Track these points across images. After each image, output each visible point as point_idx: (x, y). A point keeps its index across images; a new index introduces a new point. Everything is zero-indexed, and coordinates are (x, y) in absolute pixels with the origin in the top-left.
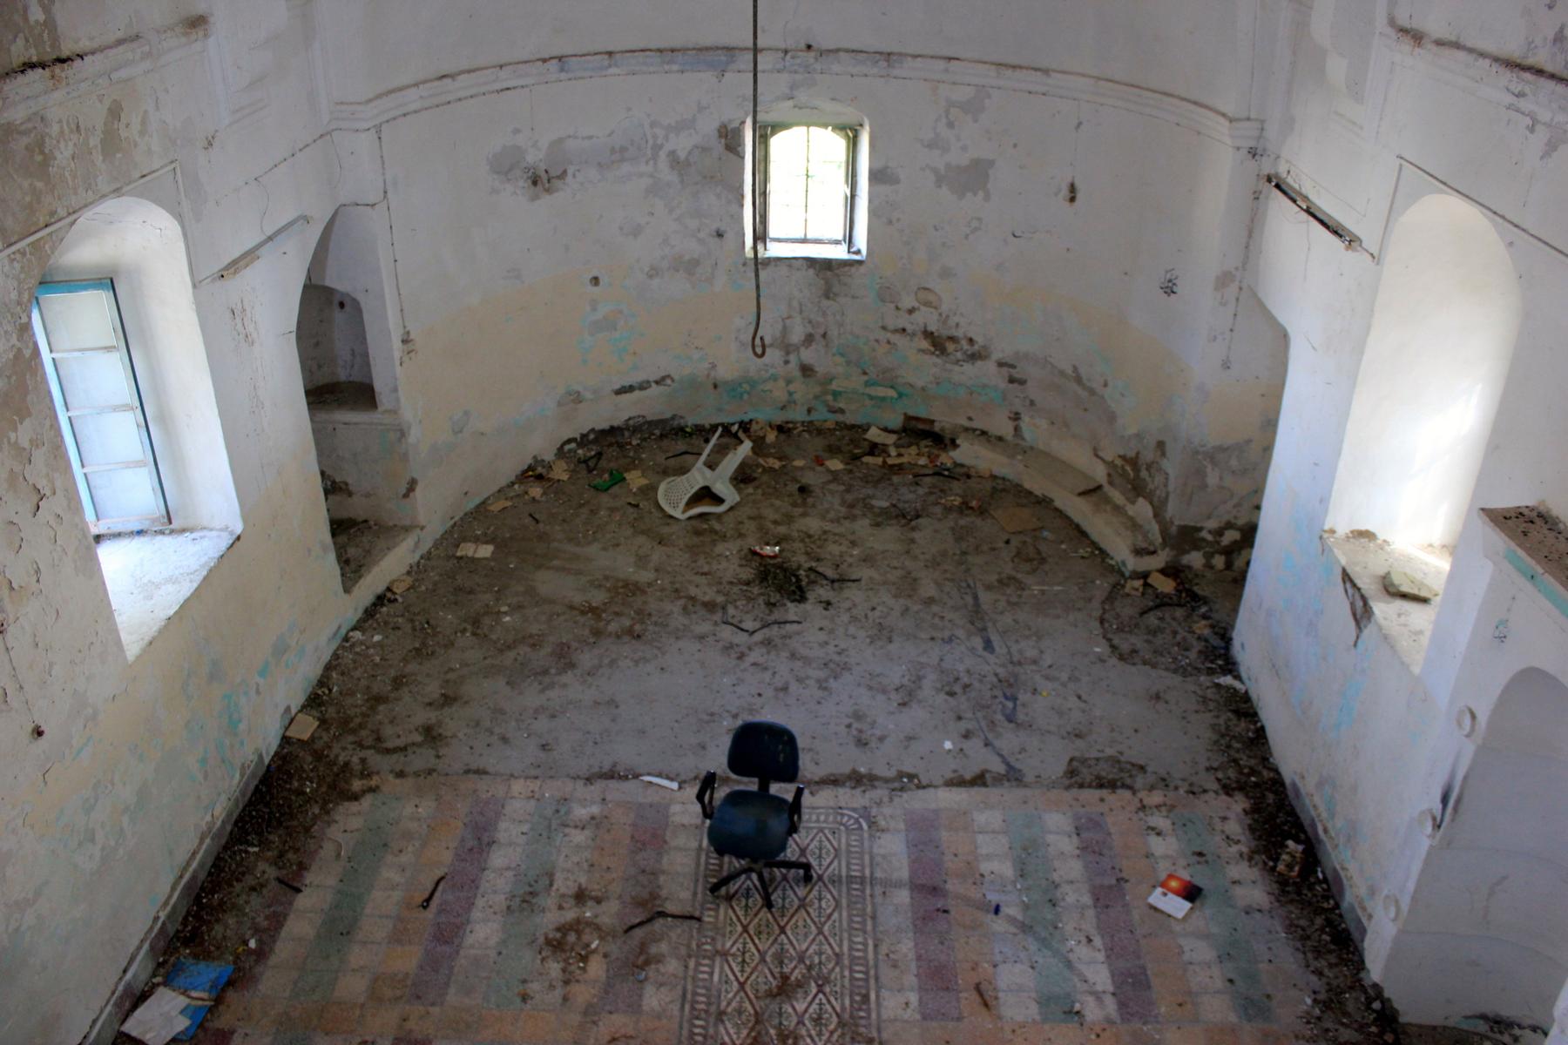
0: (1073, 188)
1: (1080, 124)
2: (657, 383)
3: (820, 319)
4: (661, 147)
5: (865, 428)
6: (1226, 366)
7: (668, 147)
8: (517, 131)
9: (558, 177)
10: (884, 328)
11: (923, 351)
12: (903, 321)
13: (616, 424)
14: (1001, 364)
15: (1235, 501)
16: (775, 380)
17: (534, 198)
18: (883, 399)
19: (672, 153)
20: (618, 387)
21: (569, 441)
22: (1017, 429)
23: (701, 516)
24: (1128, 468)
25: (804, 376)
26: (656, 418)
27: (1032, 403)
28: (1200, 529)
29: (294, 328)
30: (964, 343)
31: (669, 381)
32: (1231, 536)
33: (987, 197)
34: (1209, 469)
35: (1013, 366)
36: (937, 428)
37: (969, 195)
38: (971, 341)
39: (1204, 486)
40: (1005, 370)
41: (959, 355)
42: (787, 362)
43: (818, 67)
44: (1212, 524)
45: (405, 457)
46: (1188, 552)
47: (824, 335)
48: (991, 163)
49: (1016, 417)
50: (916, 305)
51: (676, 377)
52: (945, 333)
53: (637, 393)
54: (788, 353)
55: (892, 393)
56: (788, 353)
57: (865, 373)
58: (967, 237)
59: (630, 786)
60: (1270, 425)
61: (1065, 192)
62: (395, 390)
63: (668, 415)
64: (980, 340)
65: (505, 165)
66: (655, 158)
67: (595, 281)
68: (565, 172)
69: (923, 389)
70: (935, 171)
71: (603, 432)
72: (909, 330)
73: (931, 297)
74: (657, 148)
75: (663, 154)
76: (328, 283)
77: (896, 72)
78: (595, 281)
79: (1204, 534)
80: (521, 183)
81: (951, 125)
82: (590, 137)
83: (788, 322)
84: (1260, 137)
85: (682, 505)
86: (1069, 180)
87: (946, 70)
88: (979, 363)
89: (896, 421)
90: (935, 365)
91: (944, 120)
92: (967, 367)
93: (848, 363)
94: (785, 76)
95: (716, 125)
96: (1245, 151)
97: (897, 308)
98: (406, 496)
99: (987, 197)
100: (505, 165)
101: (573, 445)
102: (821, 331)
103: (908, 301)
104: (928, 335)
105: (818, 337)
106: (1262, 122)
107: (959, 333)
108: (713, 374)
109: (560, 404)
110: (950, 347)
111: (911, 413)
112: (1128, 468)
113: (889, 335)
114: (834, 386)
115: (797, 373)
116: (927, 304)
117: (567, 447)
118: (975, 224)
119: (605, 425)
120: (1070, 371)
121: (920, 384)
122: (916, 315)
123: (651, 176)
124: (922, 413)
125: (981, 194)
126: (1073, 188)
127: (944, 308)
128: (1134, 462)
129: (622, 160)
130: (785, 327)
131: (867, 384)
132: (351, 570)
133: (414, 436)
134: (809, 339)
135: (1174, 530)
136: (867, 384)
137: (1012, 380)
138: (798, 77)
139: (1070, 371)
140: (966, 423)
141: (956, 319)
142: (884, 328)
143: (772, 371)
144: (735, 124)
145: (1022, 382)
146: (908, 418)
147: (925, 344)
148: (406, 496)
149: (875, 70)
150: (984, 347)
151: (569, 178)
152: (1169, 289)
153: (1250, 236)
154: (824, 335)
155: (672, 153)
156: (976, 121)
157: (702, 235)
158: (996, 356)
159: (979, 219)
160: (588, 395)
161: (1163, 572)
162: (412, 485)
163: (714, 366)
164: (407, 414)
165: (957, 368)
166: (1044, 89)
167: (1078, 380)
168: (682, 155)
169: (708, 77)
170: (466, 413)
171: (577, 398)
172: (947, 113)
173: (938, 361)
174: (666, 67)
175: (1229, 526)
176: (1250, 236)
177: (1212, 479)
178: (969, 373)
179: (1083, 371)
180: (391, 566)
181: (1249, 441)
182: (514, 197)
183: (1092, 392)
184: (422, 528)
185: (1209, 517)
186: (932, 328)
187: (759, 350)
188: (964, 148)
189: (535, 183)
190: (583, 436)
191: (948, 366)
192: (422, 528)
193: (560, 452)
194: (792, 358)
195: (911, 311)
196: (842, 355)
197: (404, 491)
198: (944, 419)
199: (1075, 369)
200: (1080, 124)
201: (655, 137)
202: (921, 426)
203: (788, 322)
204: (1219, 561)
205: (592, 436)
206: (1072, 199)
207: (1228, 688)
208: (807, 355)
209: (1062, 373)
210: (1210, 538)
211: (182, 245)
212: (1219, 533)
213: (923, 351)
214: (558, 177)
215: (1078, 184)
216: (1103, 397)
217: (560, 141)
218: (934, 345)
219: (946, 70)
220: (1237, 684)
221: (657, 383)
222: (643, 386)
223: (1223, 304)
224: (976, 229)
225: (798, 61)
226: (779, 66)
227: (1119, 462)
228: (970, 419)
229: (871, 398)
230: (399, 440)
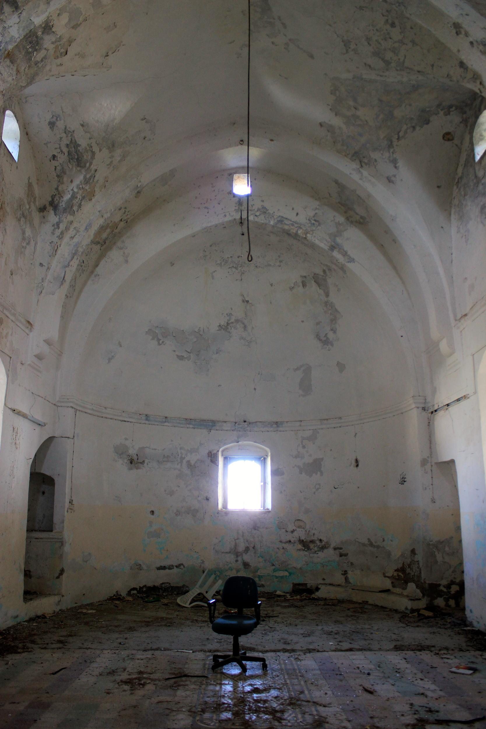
0: (357, 461)
1: (356, 434)
2: (176, 567)
3: (252, 540)
4: (184, 458)
5: (276, 591)
6: (433, 501)
7: (187, 458)
8: (126, 439)
9: (141, 463)
10: (281, 542)
11: (300, 550)
12: (289, 537)
13: (156, 584)
14: (335, 549)
15: (452, 569)
16: (232, 570)
17: (130, 469)
18: (282, 577)
19: (188, 462)
20: (159, 566)
21: (134, 589)
22: (346, 579)
23: (197, 606)
24: (400, 574)
25: (245, 568)
26: (175, 585)
27: (352, 564)
28: (439, 585)
29: (33, 457)
30: (318, 542)
31: (182, 567)
32: (455, 588)
33: (322, 474)
34: (436, 553)
35: (341, 549)
36: (309, 586)
37: (314, 475)
38: (321, 540)
39: (436, 562)
40: (337, 552)
41: (316, 549)
42: (237, 561)
43: (249, 428)
44: (444, 582)
45: (61, 557)
46: (436, 598)
47: (254, 548)
48: (322, 459)
49: (345, 573)
50: (294, 528)
51: (186, 566)
52: (309, 539)
53: (167, 570)
54: (237, 556)
55: (286, 574)
56: (237, 556)
57: (273, 565)
58: (314, 493)
59: (169, 652)
60: (458, 529)
61: (354, 463)
62: (63, 522)
63: (180, 585)
64: (324, 539)
65: (120, 451)
66: (181, 462)
67: (152, 512)
68: (144, 461)
69: (301, 569)
70: (299, 467)
71: (150, 587)
72: (292, 541)
73: (301, 524)
74: (182, 459)
75: (184, 462)
76: (43, 471)
77: (280, 429)
78: (152, 512)
79: (442, 588)
80: (126, 461)
81: (304, 447)
82: (155, 449)
83: (237, 541)
84: (425, 403)
85: (189, 602)
86: (355, 458)
87: (300, 426)
88: (325, 551)
89: (288, 587)
90: (305, 556)
91: (301, 446)
92: (320, 554)
93: (265, 561)
94: (235, 432)
95: (207, 451)
96: (421, 409)
97: (287, 531)
98: (58, 577)
99: (322, 474)
100: (120, 451)
101: (135, 592)
102: (252, 545)
103: (291, 528)
104: (301, 542)
105: (251, 548)
106: (425, 397)
107: (315, 538)
108: (202, 565)
109: (131, 568)
110: (312, 546)
111: (295, 582)
112: (400, 574)
113: (284, 545)
114: (259, 573)
115: (242, 567)
116: (300, 527)
117: (133, 592)
118: (317, 486)
119: (150, 584)
120: (367, 542)
121: (299, 566)
122: (295, 533)
123: (179, 470)
124: (301, 580)
125: (319, 473)
126: (357, 461)
127: (308, 527)
128: (402, 570)
129: (168, 461)
130: (236, 543)
131: (274, 571)
132: (29, 594)
133: (67, 548)
134: (247, 549)
135: (427, 586)
136: (274, 571)
137: (341, 555)
138: (241, 433)
139: (367, 542)
140: (322, 582)
141: (313, 532)
142: (281, 542)
143: (230, 565)
144: (215, 452)
145: (346, 555)
146: (295, 585)
147: (300, 546)
148: (58, 577)
149: (272, 429)
150: (327, 543)
151: (145, 464)
152: (403, 481)
153: (430, 443)
154: (254, 548)
155: (188, 462)
156: (314, 444)
157: (199, 499)
158: (333, 545)
159: (319, 484)
160: (144, 567)
161: (425, 609)
162: (62, 571)
163: (203, 562)
164: (67, 535)
165: (315, 555)
166: (340, 425)
167: (371, 544)
168: (193, 463)
169: (205, 431)
170: (90, 554)
171: (139, 567)
172: (302, 442)
173: (307, 553)
174: (188, 426)
175: (452, 583)
176: (430, 443)
177: (439, 557)
178: (322, 555)
179: (373, 541)
180: (45, 605)
181: (452, 538)
182: (121, 465)
183: (378, 547)
184: (63, 596)
185: (442, 579)
186: (303, 538)
187: (250, 259)
188: (310, 456)
189: (131, 463)
190: (140, 588)
191: (311, 555)
192: (63, 596)
193: (129, 593)
194: (239, 559)
195: (292, 532)
196: (262, 557)
197: (57, 575)
198: (311, 582)
199: (369, 539)
200: (356, 434)
201: (181, 453)
202: (301, 587)
203: (237, 541)
204: (452, 602)
205: (144, 589)
206: (357, 466)
207: (469, 630)
208: (247, 558)
209: (364, 545)
210: (445, 590)
211: (5, 387)
212: (448, 587)
213: (300, 550)
214: (141, 463)
215: (359, 458)
216: (383, 547)
217: (143, 448)
218: (304, 546)
219: (300, 426)
220: (474, 628)
221: (176, 567)
222: (170, 567)
223: (426, 473)
224: (318, 489)
225: (241, 426)
226: (234, 428)
227: (395, 574)
228: (324, 579)
229: (277, 577)
230: (60, 547)
